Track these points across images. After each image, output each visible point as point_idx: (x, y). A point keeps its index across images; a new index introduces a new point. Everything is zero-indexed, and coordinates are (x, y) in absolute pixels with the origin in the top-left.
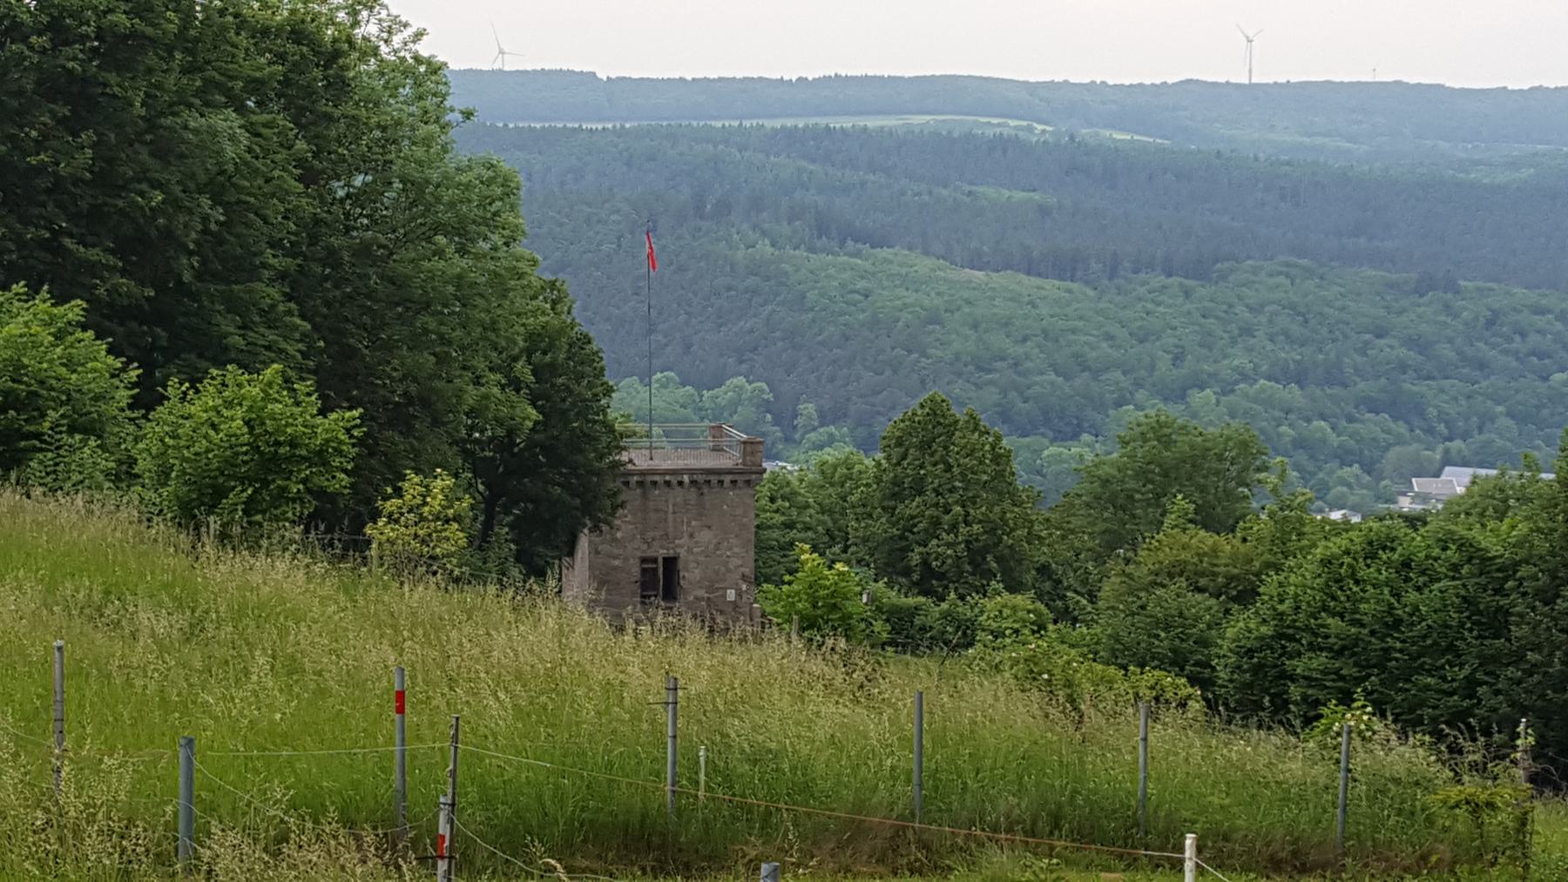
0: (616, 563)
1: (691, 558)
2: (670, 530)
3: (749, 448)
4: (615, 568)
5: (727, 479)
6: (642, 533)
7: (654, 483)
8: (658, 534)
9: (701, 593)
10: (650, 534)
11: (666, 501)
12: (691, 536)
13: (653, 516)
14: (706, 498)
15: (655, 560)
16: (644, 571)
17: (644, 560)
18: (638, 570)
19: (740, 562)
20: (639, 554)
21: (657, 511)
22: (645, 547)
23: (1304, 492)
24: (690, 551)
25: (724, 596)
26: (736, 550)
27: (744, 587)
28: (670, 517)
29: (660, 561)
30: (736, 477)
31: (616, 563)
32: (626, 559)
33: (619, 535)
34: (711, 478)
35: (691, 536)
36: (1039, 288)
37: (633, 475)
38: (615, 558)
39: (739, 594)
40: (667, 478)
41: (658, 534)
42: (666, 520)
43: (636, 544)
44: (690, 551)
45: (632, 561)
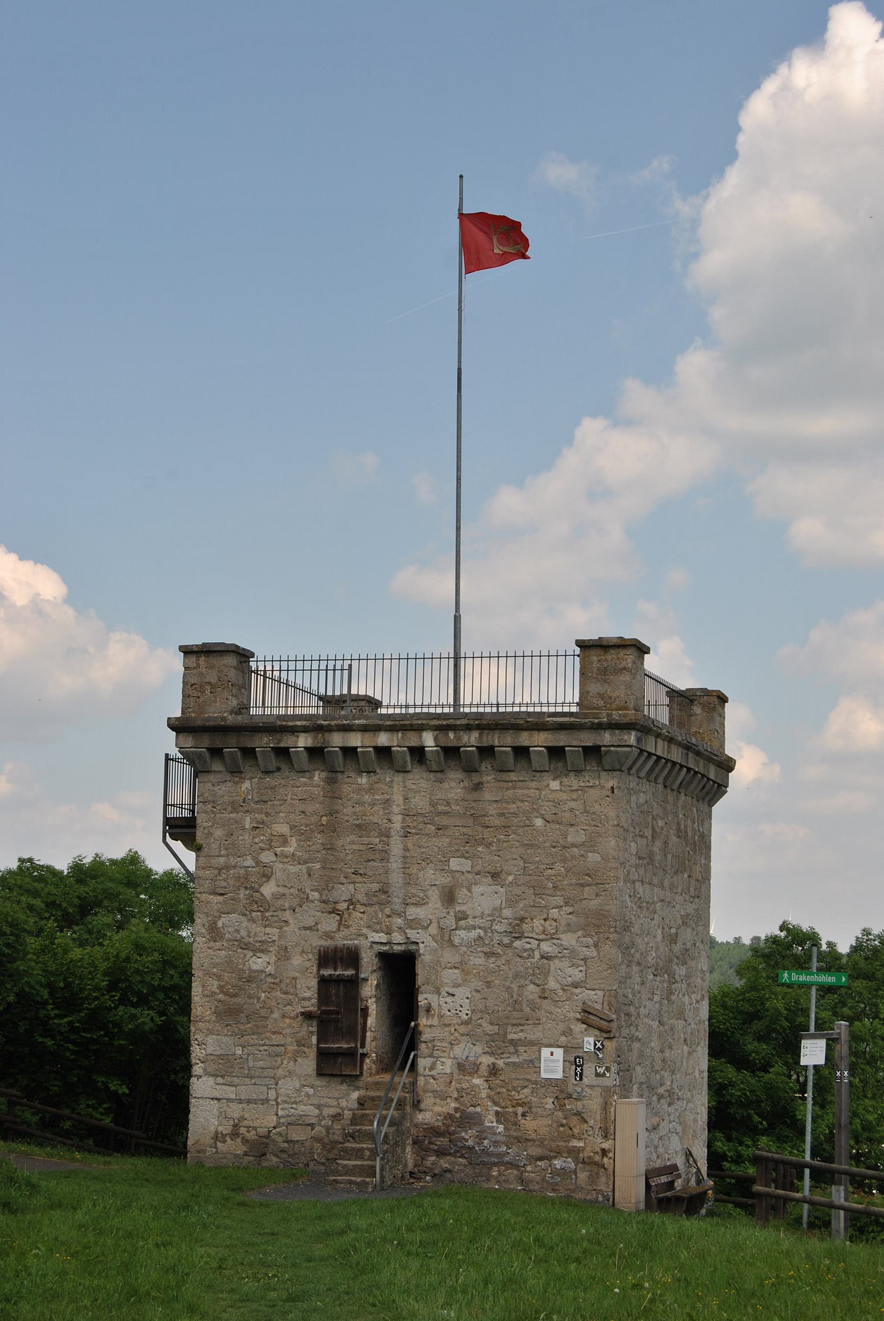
0: (258, 963)
1: (449, 956)
2: (396, 879)
3: (594, 657)
4: (252, 978)
5: (539, 741)
6: (326, 886)
7: (349, 752)
8: (362, 890)
9: (476, 1052)
10: (343, 892)
11: (387, 802)
12: (449, 898)
13: (349, 843)
14: (487, 795)
15: (352, 957)
16: (324, 983)
17: (326, 958)
18: (314, 983)
19: (577, 975)
20: (317, 942)
21: (361, 828)
22: (330, 923)
23: (382, 937)
24: (445, 938)
25: (534, 1064)
26: (568, 939)
27: (589, 1043)
28: (396, 846)
29: (369, 961)
30: (561, 739)
31: (258, 963)
32: (284, 954)
33: (268, 890)
34: (494, 739)
35: (449, 898)
36: (340, 765)
37: (294, 731)
38: (261, 949)
39: (576, 1063)
40: (383, 739)
41: (362, 890)
42: (385, 856)
43: (310, 914)
44: (445, 938)
45: (297, 961)
